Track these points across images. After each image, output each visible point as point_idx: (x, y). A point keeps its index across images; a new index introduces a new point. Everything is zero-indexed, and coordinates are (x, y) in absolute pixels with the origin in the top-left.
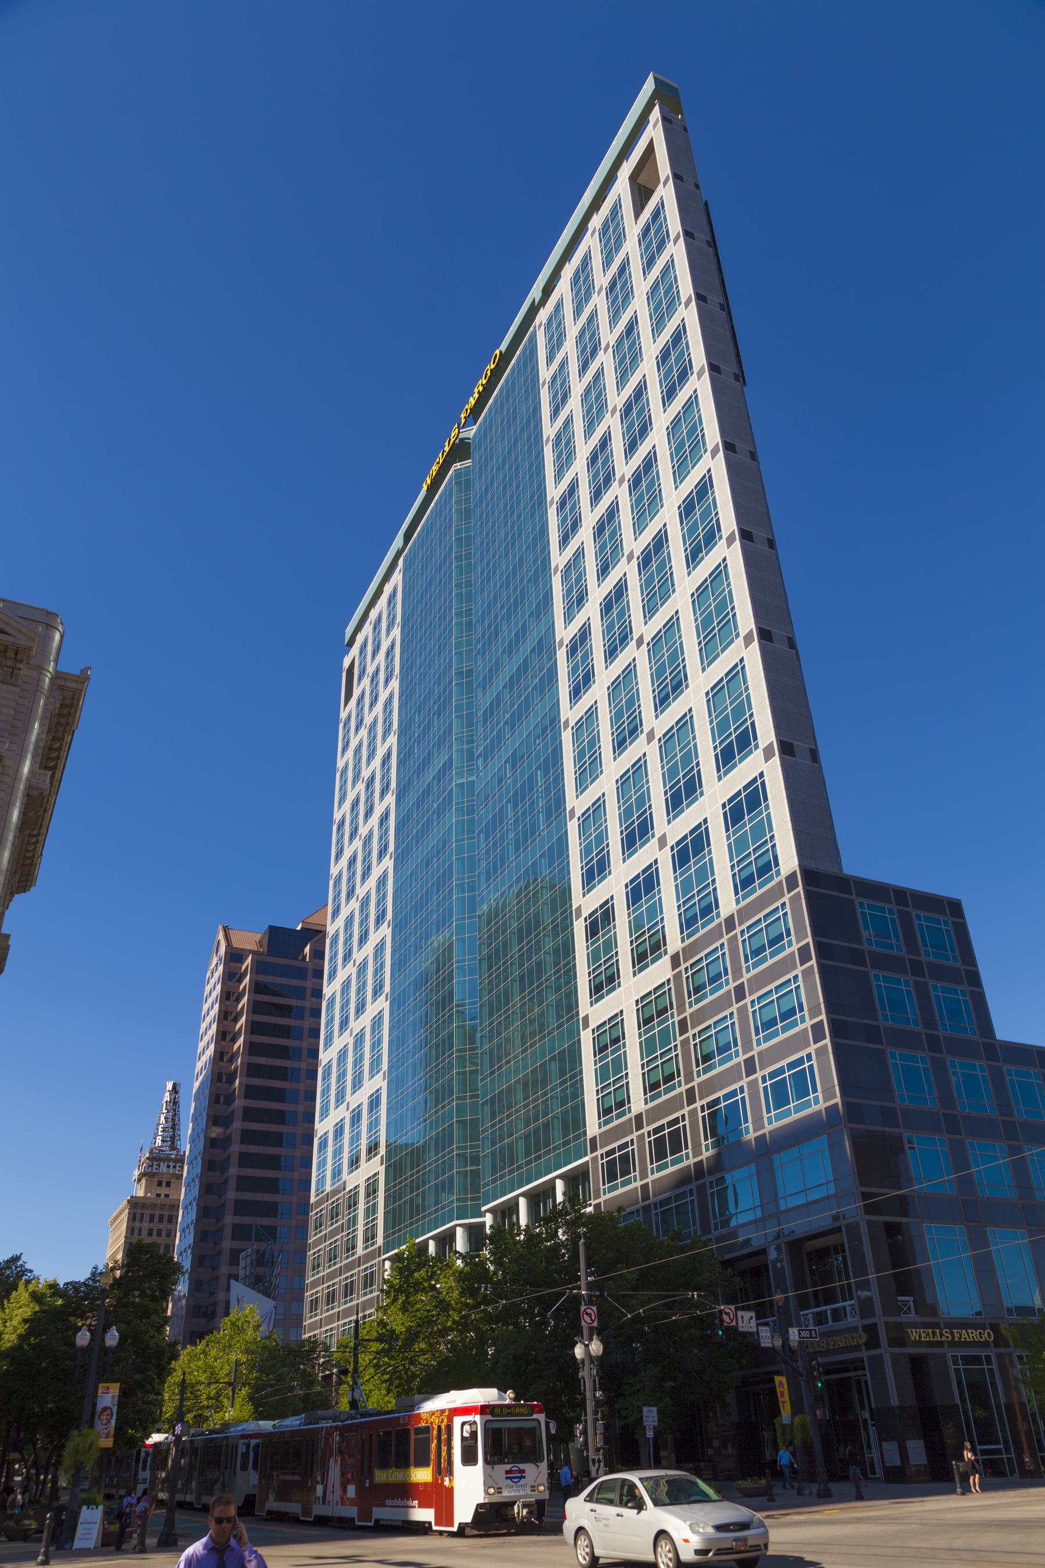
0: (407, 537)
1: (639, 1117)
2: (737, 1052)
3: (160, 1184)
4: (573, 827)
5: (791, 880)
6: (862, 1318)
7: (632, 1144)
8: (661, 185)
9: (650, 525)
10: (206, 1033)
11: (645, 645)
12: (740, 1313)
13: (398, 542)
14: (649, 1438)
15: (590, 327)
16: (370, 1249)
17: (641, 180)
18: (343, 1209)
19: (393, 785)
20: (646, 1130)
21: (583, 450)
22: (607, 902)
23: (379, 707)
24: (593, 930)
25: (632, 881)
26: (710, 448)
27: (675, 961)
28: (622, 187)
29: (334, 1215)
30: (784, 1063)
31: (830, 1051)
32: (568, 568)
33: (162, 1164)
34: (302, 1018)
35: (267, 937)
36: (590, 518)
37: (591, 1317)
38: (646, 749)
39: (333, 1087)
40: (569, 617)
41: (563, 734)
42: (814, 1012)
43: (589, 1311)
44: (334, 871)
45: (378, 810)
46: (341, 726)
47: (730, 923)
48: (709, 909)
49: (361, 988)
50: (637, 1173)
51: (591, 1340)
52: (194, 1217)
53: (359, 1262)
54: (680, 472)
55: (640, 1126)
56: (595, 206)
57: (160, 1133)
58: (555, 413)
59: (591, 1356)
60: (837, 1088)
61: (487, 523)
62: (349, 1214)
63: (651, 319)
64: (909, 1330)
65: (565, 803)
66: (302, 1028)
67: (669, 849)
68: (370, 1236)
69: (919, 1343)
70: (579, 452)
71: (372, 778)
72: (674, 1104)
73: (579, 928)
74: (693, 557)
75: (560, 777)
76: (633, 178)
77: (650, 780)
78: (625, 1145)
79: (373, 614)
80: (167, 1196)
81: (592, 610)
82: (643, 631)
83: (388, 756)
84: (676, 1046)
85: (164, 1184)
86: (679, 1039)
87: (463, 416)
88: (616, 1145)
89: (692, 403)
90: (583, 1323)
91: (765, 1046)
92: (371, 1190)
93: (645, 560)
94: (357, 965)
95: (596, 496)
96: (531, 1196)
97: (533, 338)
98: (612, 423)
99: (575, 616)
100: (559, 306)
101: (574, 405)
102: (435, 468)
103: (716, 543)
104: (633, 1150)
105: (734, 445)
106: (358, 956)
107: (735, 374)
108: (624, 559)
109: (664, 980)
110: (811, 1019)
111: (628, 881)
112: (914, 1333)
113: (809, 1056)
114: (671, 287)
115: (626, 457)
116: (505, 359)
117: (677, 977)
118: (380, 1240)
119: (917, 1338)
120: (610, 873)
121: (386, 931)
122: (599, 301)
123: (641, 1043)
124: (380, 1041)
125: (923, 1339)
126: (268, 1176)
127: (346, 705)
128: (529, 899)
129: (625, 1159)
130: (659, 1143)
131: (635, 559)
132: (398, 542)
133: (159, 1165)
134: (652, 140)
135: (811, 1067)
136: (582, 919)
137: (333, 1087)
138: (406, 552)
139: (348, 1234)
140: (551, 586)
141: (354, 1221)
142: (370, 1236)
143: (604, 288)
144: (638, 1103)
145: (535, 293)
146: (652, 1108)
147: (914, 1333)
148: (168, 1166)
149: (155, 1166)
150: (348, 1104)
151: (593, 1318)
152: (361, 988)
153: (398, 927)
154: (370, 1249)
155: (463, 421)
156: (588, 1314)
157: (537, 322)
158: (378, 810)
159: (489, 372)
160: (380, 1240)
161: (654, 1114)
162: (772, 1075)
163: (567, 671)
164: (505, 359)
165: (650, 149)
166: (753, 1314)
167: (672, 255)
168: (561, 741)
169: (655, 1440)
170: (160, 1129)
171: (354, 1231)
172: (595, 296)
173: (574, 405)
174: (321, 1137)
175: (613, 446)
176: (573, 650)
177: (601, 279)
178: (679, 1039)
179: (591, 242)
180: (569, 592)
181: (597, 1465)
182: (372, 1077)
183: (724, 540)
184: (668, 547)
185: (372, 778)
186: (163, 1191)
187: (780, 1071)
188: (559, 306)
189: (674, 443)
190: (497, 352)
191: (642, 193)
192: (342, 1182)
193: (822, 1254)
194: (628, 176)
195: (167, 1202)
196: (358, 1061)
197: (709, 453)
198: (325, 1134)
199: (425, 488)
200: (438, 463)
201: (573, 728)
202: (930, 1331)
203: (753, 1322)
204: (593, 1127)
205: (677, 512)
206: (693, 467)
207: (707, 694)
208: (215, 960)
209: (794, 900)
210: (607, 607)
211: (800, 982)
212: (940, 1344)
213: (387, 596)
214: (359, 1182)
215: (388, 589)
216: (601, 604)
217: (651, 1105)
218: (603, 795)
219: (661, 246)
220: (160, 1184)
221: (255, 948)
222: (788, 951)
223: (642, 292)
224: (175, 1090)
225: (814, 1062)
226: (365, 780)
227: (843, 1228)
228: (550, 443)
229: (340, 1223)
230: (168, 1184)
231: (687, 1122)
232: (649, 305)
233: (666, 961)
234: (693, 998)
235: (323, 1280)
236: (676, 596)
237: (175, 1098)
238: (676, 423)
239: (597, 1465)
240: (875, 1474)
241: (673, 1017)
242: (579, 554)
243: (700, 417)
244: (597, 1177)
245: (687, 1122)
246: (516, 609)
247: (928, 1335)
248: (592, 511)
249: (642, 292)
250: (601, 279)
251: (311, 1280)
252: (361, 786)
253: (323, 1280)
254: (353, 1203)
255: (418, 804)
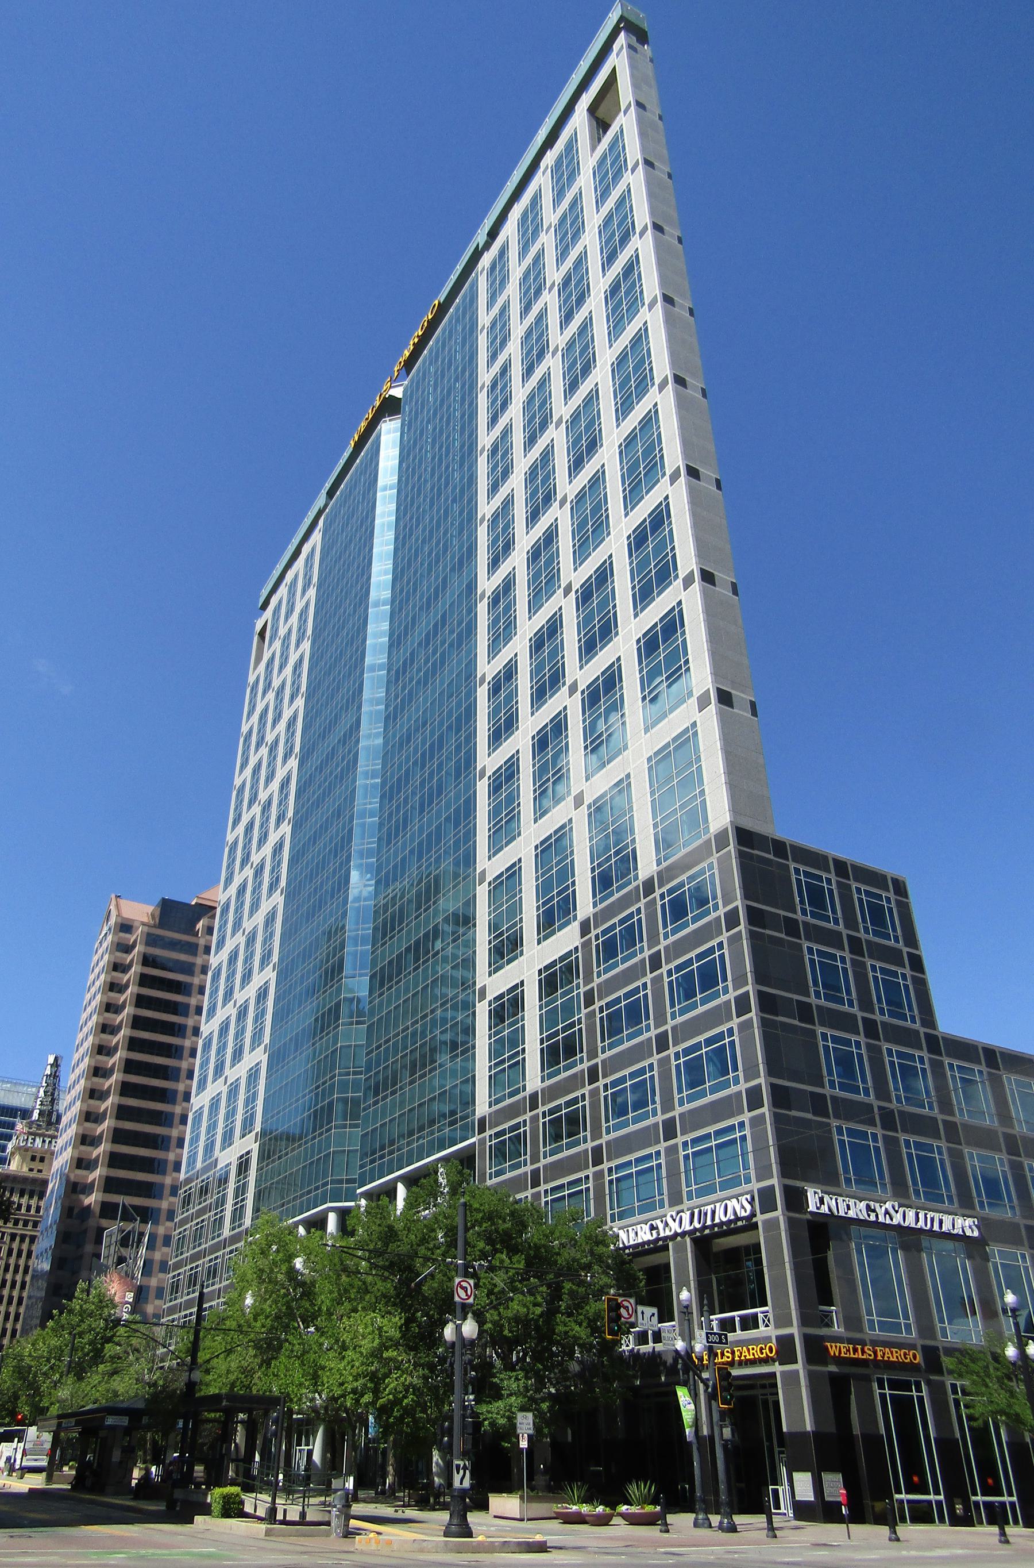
0: (330, 494)
1: (534, 1097)
2: (655, 1110)
3: (33, 1158)
4: (482, 788)
5: (721, 839)
6: (777, 1327)
7: (525, 1125)
8: (622, 113)
9: (593, 555)
10: (90, 1004)
11: (579, 693)
12: (640, 1308)
13: (321, 500)
14: (523, 1449)
15: (542, 391)
16: (237, 1230)
17: (601, 113)
18: (213, 1187)
19: (297, 749)
20: (541, 1110)
21: (522, 463)
22: (516, 987)
23: (282, 726)
24: (495, 788)
25: (547, 968)
26: (657, 381)
27: (585, 928)
28: (580, 117)
29: (204, 1191)
30: (701, 1038)
31: (755, 1025)
32: (495, 517)
33: (37, 1139)
34: (186, 1015)
35: (159, 909)
36: (525, 540)
37: (466, 1292)
38: (568, 702)
39: (213, 1060)
40: (494, 649)
41: (478, 783)
42: (740, 980)
43: (464, 1284)
44: (230, 838)
45: (273, 838)
46: (242, 740)
47: (649, 887)
48: (628, 861)
49: (249, 958)
50: (528, 1157)
51: (465, 1319)
52: (53, 1243)
53: (225, 1244)
54: (632, 496)
55: (534, 1106)
56: (550, 142)
57: (38, 1107)
58: (494, 489)
59: (463, 1339)
60: (761, 1067)
61: (412, 505)
62: (219, 1193)
63: (615, 397)
64: (828, 1344)
65: (475, 761)
66: (185, 1026)
67: (586, 808)
68: (238, 1214)
69: (839, 1360)
70: (519, 410)
71: (269, 802)
72: (574, 1082)
73: (482, 788)
74: (644, 596)
75: (471, 834)
76: (592, 110)
77: (569, 735)
78: (517, 1127)
79: (289, 576)
80: (40, 1171)
81: (519, 646)
82: (578, 677)
83: (294, 718)
84: (580, 1019)
85: (38, 1159)
86: (584, 1011)
87: (396, 369)
88: (506, 1126)
89: (650, 420)
90: (457, 1299)
91: (680, 1019)
92: (243, 1166)
93: (585, 595)
94: (238, 1006)
95: (533, 517)
96: (410, 1181)
97: (475, 285)
98: (557, 436)
99: (500, 650)
100: (503, 252)
101: (515, 412)
102: (363, 424)
103: (670, 583)
104: (525, 1132)
105: (712, 575)
106: (239, 997)
107: (678, 237)
108: (560, 592)
109: (572, 947)
110: (735, 990)
111: (538, 842)
112: (834, 1348)
113: (731, 1031)
114: (642, 361)
115: (570, 475)
116: (443, 309)
117: (586, 945)
118: (248, 1222)
119: (837, 1354)
120: (522, 954)
121: (278, 899)
122: (547, 240)
123: (542, 1050)
124: (263, 1012)
125: (843, 1355)
126: (145, 1130)
127: (233, 829)
128: (430, 864)
129: (517, 1140)
130: (556, 1123)
131: (573, 592)
132: (321, 500)
133: (34, 1140)
134: (615, 67)
135: (732, 1043)
136: (486, 1002)
137: (213, 1060)
138: (327, 510)
139: (216, 1214)
140: (476, 655)
141: (221, 1202)
142: (238, 1214)
143: (560, 349)
144: (534, 1080)
145: (481, 237)
146: (549, 1087)
147: (834, 1348)
148: (44, 1141)
149: (30, 1140)
150: (226, 1078)
151: (469, 1293)
152: (249, 958)
153: (290, 896)
154: (237, 1230)
155: (396, 374)
156: (463, 1288)
157: (480, 266)
158: (273, 838)
159: (426, 324)
160: (248, 1222)
161: (551, 1093)
162: (687, 1052)
163: (487, 623)
164: (443, 309)
165: (612, 79)
166: (655, 1310)
167: (646, 322)
168: (475, 792)
169: (530, 1450)
170: (39, 1103)
171: (222, 1211)
172: (543, 235)
173: (515, 412)
174: (196, 1112)
175: (560, 543)
176: (495, 689)
177: (550, 216)
178: (584, 1011)
179: (542, 180)
180: (495, 541)
181: (461, 1472)
182: (253, 1050)
183: (680, 581)
184: (613, 582)
185: (269, 802)
186: (36, 1165)
187: (697, 1047)
188: (503, 252)
189: (619, 379)
190: (436, 302)
191: (601, 124)
192: (213, 1159)
193: (734, 1256)
194: (586, 108)
195: (40, 1176)
196: (240, 1033)
197: (667, 478)
198: (201, 1108)
199: (352, 444)
200: (367, 419)
201: (489, 778)
202: (851, 1346)
203: (655, 1319)
204: (482, 1107)
205: (626, 543)
206: (647, 493)
207: (649, 759)
208: (105, 929)
209: (735, 939)
210: (538, 644)
211: (747, 1132)
212: (864, 1363)
213: (305, 557)
214: (232, 1160)
215: (306, 549)
216: (531, 640)
217: (548, 1083)
218: (518, 752)
219: (625, 239)
220: (33, 1158)
221: (145, 920)
222: (723, 998)
223: (606, 361)
224: (56, 1064)
225: (726, 951)
226: (269, 744)
227: (760, 1224)
228: (486, 523)
229: (208, 1202)
230: (42, 1160)
231: (587, 1102)
232: (613, 380)
233: (575, 927)
234: (607, 1042)
235: (179, 1308)
236: (611, 539)
237: (56, 1072)
238: (630, 441)
239: (461, 1472)
240: (780, 1509)
241: (578, 988)
242: (508, 503)
243: (659, 435)
244: (485, 1164)
245: (587, 1102)
246: (434, 674)
247: (848, 1350)
248: (527, 533)
249: (606, 361)
250: (550, 216)
251: (180, 1218)
252: (257, 809)
253: (179, 1308)
254: (223, 1181)
255: (320, 769)
